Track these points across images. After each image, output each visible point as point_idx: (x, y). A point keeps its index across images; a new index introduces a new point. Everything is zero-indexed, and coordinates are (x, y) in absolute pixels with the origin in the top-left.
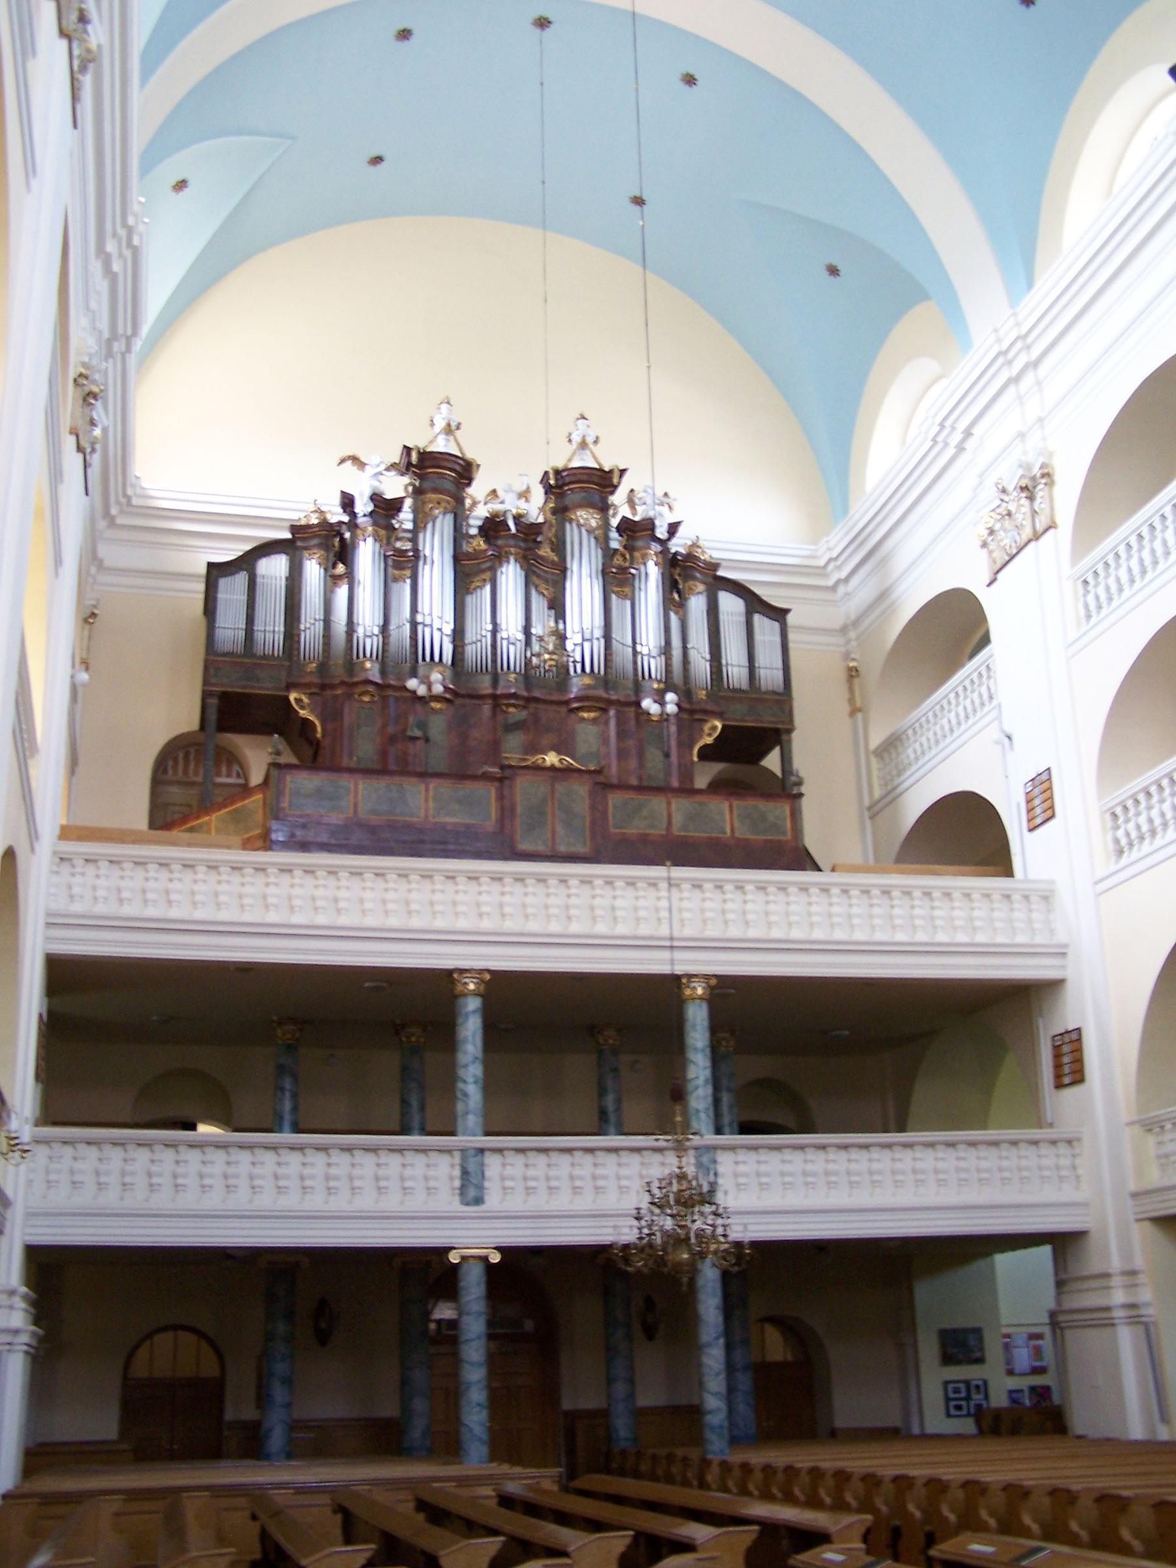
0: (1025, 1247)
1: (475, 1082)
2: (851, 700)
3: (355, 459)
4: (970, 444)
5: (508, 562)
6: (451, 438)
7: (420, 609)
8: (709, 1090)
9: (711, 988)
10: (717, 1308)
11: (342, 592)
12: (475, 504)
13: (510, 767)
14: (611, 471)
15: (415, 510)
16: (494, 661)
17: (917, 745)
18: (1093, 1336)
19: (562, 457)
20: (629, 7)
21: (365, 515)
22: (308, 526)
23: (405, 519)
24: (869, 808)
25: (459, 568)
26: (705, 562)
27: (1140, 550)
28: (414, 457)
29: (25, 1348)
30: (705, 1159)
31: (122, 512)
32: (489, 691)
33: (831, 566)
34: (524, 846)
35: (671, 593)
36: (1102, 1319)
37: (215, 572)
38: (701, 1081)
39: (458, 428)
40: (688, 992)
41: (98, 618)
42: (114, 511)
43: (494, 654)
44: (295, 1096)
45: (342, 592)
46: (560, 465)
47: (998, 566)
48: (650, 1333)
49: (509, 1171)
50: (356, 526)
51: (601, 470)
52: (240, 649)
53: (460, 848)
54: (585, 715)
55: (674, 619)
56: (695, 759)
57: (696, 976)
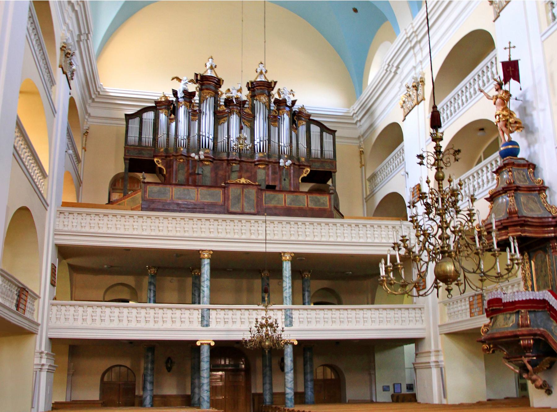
1: (207, 287)
2: (361, 162)
4: (399, 72)
6: (213, 71)
7: (201, 130)
8: (291, 290)
10: (291, 361)
11: (173, 124)
12: (222, 94)
14: (271, 82)
15: (200, 96)
16: (228, 148)
17: (381, 177)
19: (253, 77)
21: (181, 98)
22: (161, 102)
23: (196, 99)
24: (366, 198)
25: (216, 116)
26: (306, 114)
28: (199, 78)
29: (47, 370)
30: (288, 313)
31: (97, 97)
32: (226, 158)
34: (231, 210)
35: (293, 125)
36: (427, 366)
37: (128, 118)
38: (288, 287)
39: (216, 67)
40: (284, 258)
41: (89, 133)
42: (93, 96)
43: (228, 145)
44: (154, 292)
45: (173, 124)
46: (253, 80)
49: (218, 316)
50: (178, 102)
51: (268, 82)
53: (210, 210)
54: (261, 166)
56: (300, 181)
57: (287, 253)
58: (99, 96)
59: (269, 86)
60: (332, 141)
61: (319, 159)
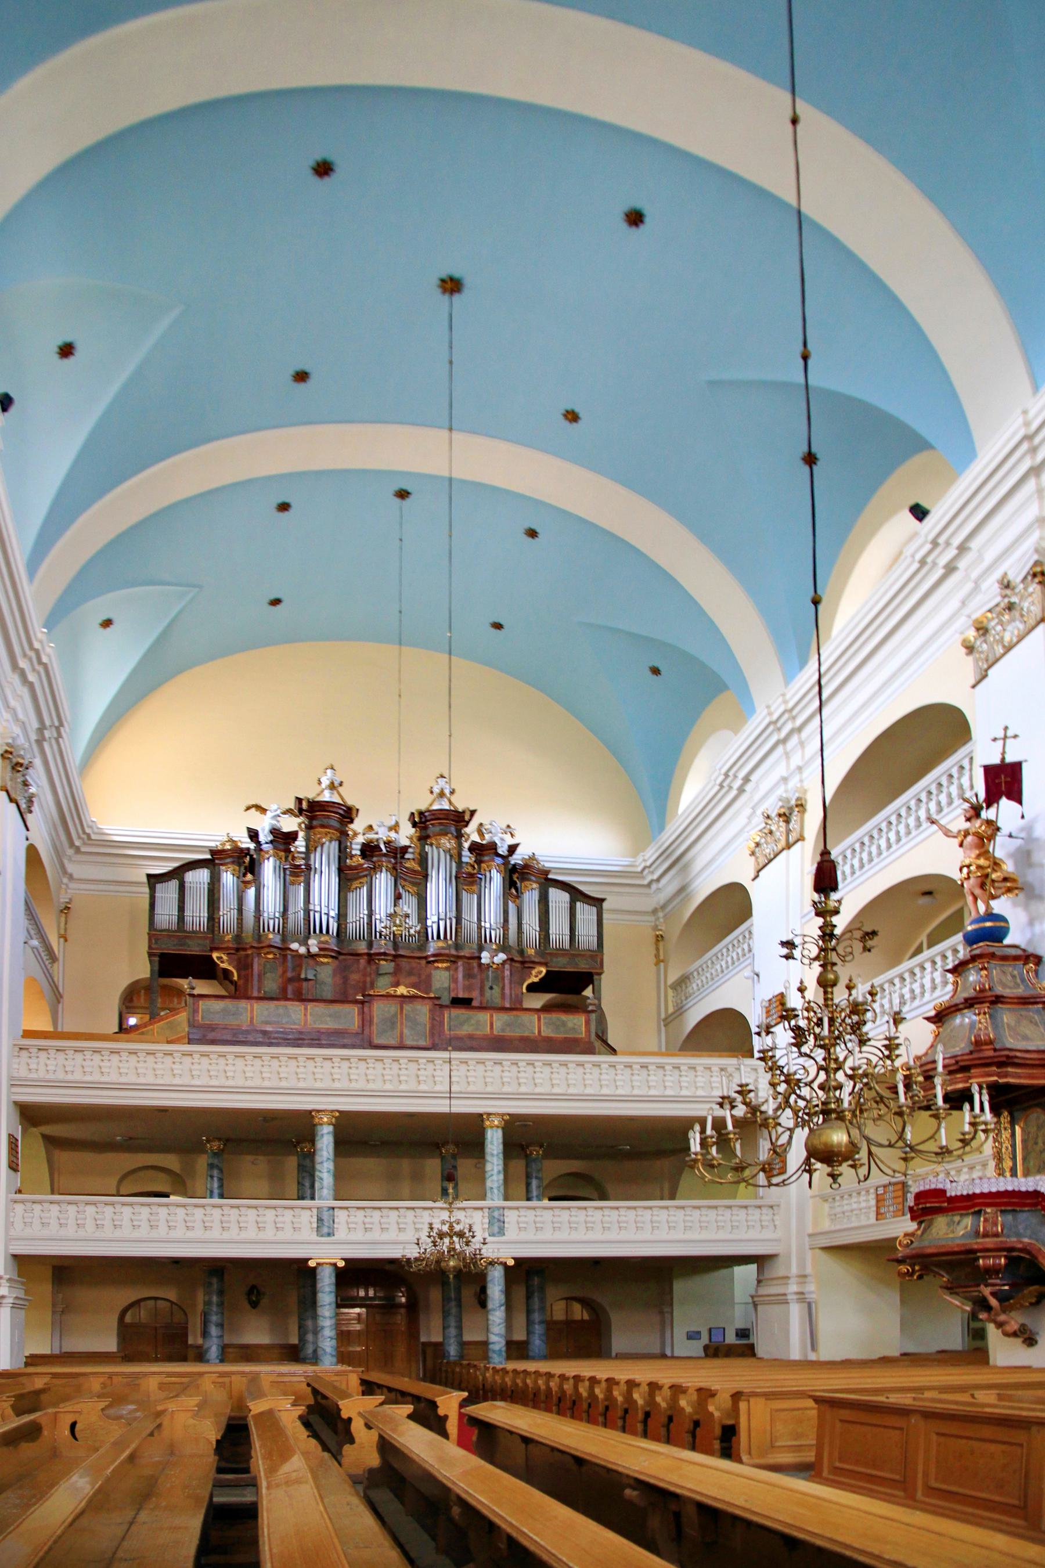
0: (747, 1263)
1: (328, 1172)
2: (657, 956)
3: (258, 808)
4: (748, 787)
5: (381, 872)
6: (335, 792)
9: (506, 1122)
11: (251, 892)
12: (356, 834)
13: (370, 995)
14: (464, 812)
15: (307, 840)
17: (699, 982)
18: (776, 1309)
20: (446, 474)
21: (267, 843)
22: (223, 851)
23: (300, 845)
24: (664, 1020)
25: (342, 875)
26: (539, 870)
27: (861, 853)
28: (305, 805)
32: (366, 951)
33: (646, 871)
34: (377, 1041)
36: (782, 1300)
37: (153, 880)
39: (341, 784)
40: (487, 1123)
42: (77, 843)
44: (220, 1180)
45: (251, 892)
46: (423, 807)
47: (761, 865)
48: (254, 1305)
51: (456, 811)
52: (174, 927)
54: (440, 965)
55: (512, 907)
56: (524, 990)
58: (90, 842)
59: (458, 819)
60: (595, 918)
61: (566, 950)
